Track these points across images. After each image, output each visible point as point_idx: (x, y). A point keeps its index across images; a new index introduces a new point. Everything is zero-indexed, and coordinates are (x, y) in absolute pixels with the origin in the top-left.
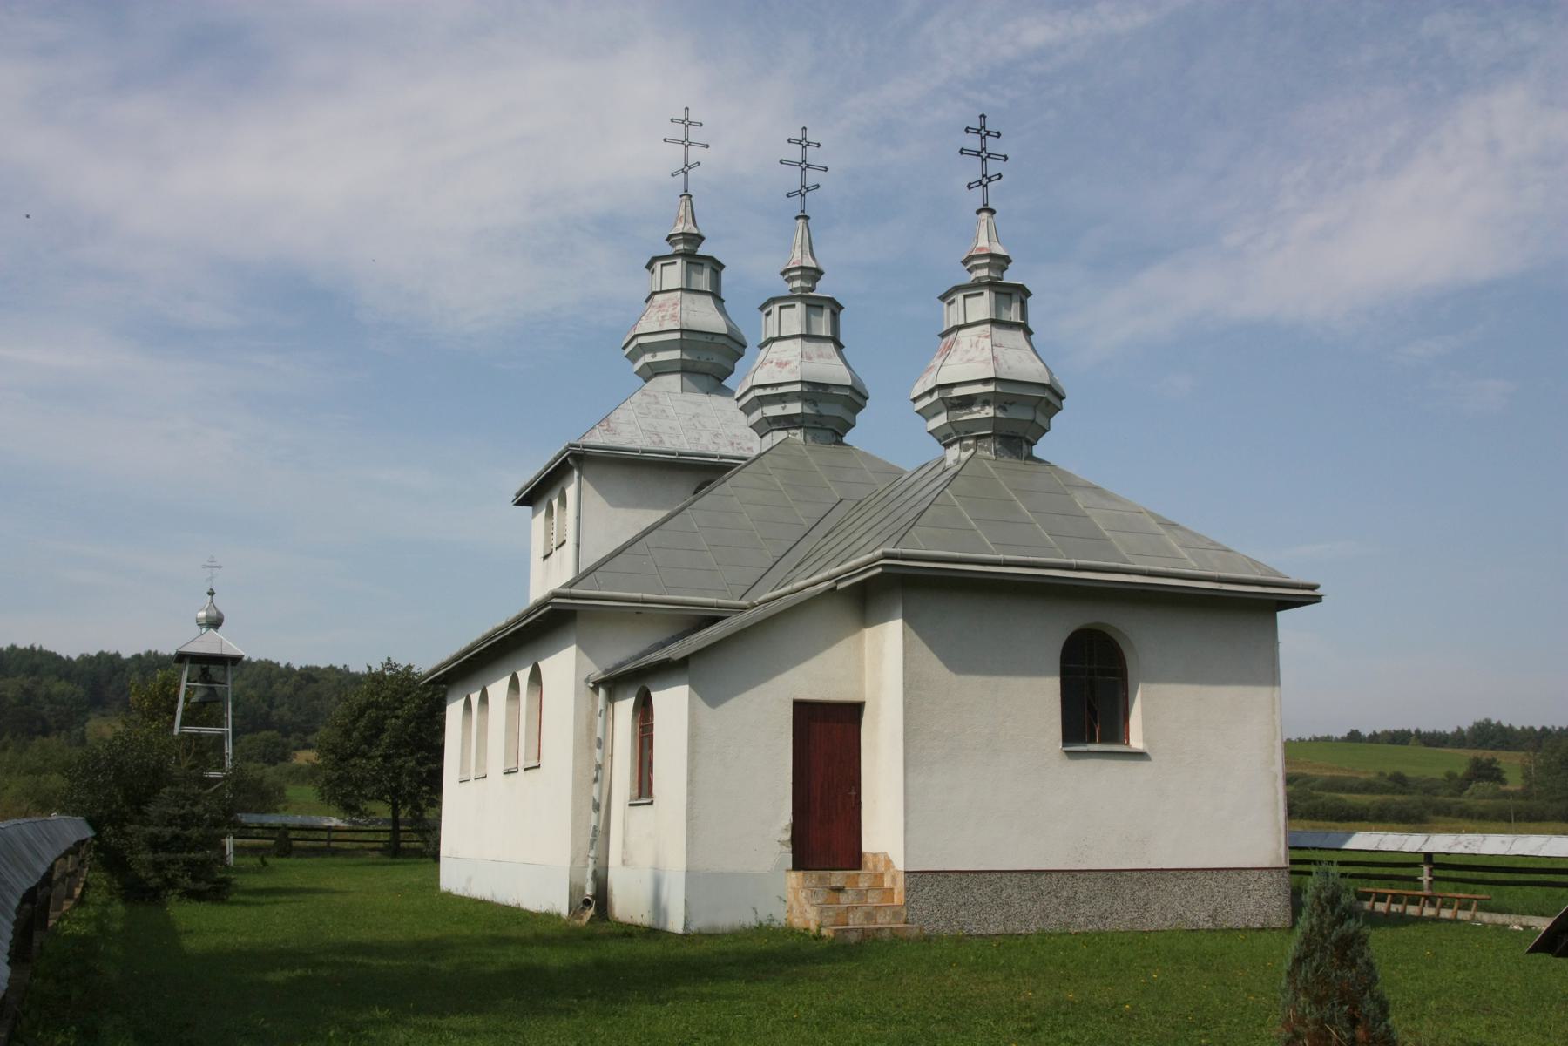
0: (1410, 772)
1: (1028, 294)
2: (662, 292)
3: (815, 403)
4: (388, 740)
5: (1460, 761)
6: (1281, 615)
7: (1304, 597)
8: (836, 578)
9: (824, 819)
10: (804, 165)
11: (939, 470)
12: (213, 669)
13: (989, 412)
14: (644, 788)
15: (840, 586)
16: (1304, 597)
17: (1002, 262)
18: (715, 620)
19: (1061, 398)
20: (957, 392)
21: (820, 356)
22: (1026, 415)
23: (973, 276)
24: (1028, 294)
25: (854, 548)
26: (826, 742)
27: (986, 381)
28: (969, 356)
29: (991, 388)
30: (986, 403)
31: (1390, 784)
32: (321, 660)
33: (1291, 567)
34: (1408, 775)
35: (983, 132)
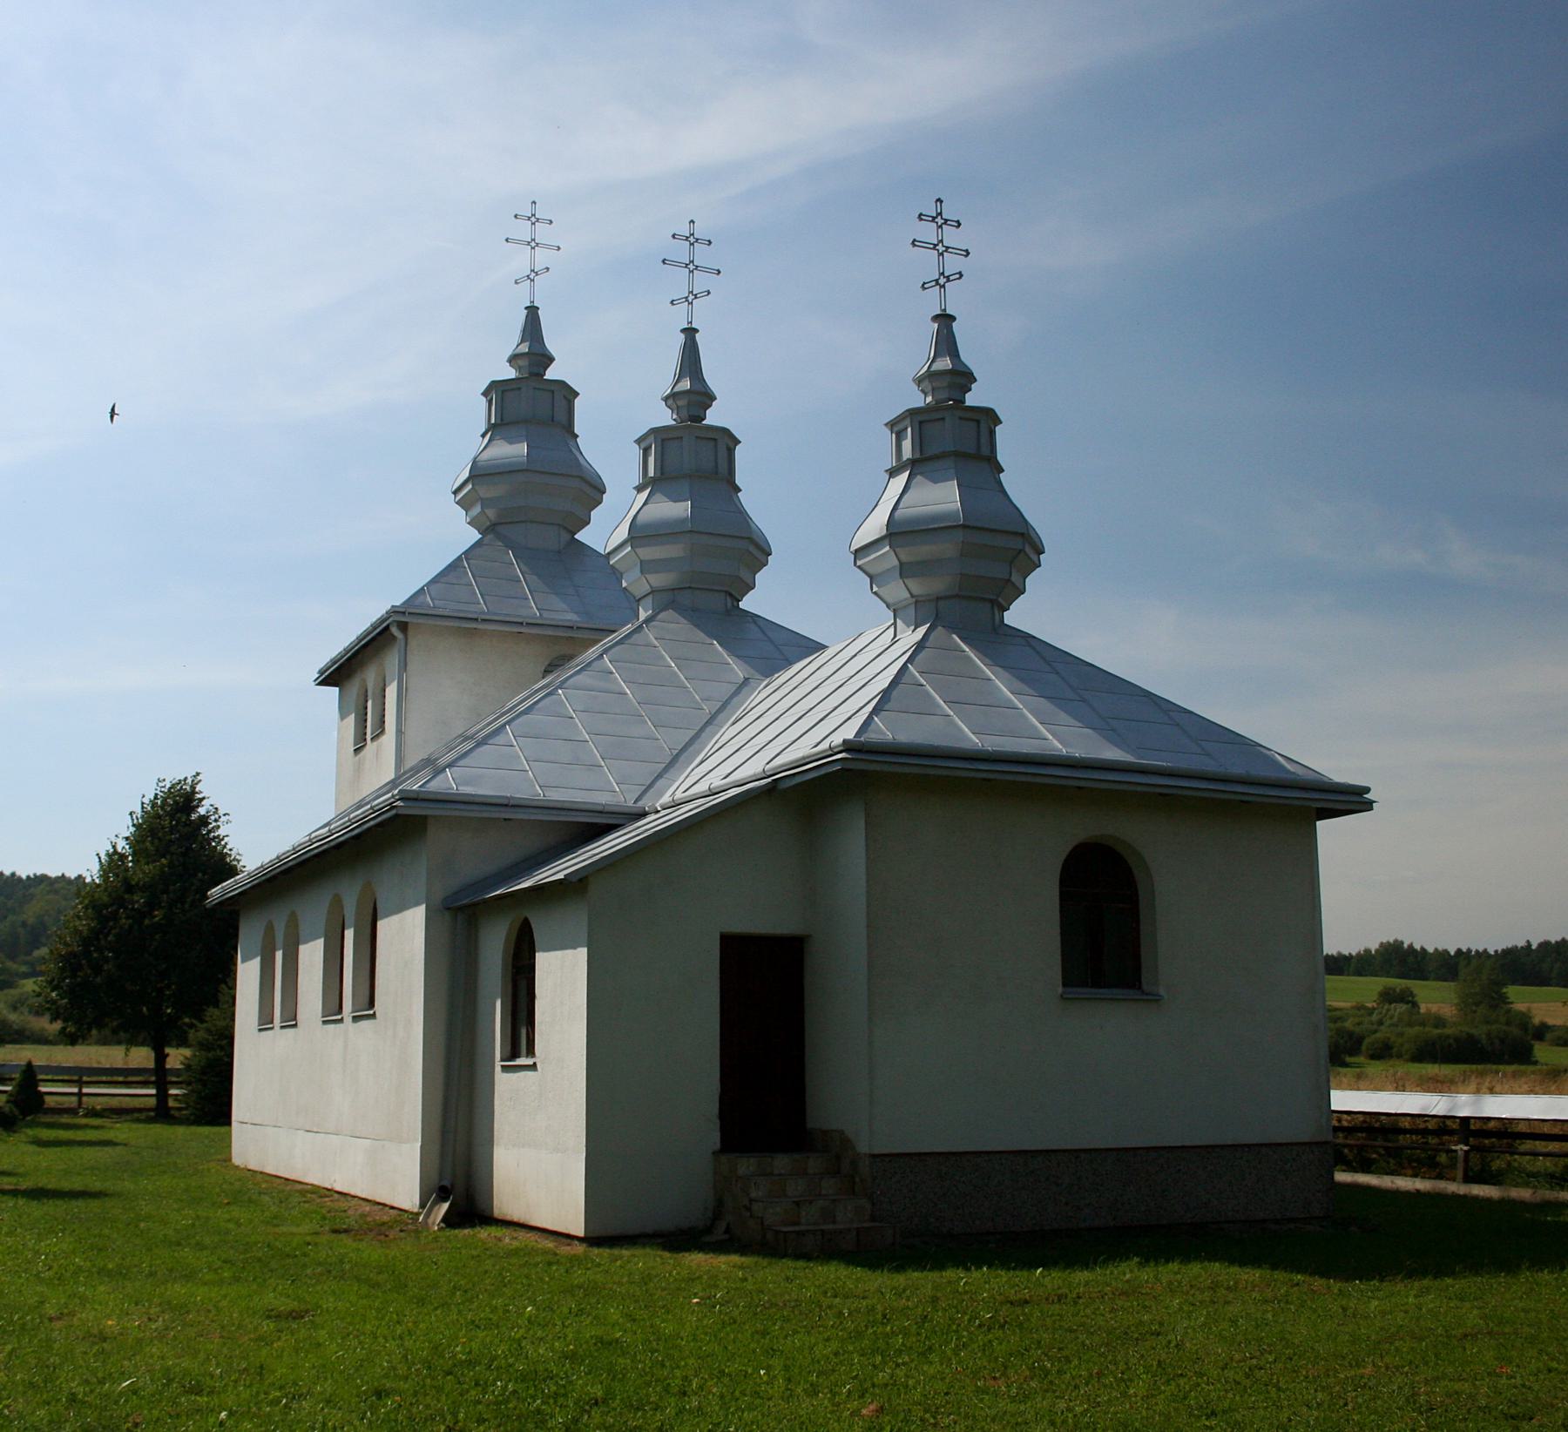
1: (997, 421)
7: (1351, 800)
16: (1351, 800)
24: (997, 421)
33: (1337, 769)
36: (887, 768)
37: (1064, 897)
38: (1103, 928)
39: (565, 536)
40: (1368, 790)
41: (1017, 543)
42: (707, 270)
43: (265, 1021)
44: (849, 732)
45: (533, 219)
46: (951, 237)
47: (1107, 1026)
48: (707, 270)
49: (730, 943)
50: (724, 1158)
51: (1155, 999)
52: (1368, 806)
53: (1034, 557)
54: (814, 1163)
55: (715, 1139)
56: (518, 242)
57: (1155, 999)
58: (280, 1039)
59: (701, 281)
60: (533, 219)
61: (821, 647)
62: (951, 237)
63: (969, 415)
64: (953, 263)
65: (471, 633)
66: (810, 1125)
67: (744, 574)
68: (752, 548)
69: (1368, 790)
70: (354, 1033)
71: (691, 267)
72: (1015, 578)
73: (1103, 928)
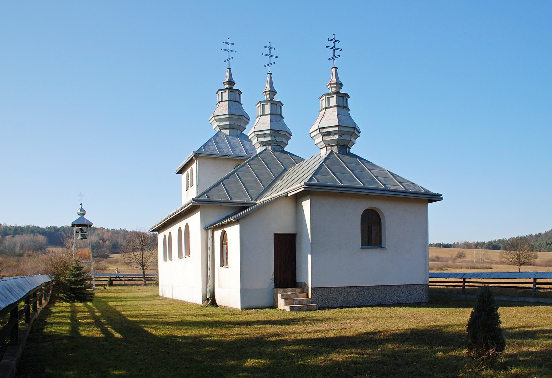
0: (440, 255)
1: (349, 97)
2: (222, 101)
3: (275, 137)
4: (142, 245)
5: (454, 252)
6: (430, 205)
7: (437, 198)
8: (288, 193)
9: (286, 273)
10: (270, 56)
11: (319, 157)
12: (84, 229)
13: (336, 137)
14: (224, 262)
15: (289, 195)
16: (437, 198)
17: (340, 86)
18: (246, 208)
19: (359, 133)
20: (325, 130)
21: (276, 121)
22: (348, 138)
23: (330, 91)
24: (349, 97)
25: (281, 188)
26: (286, 248)
27: (335, 126)
28: (330, 118)
29: (337, 129)
30: (335, 134)
31: (435, 259)
32: (117, 227)
33: (434, 190)
34: (440, 256)
35: (334, 40)
36: (314, 190)
37: (362, 224)
38: (372, 232)
39: (239, 132)
40: (441, 195)
41: (352, 130)
42: (274, 56)
43: (165, 259)
44: (306, 181)
45: (270, 48)
46: (337, 45)
47: (372, 255)
48: (274, 56)
49: (276, 235)
50: (275, 289)
51: (385, 249)
52: (442, 199)
53: (358, 134)
54: (298, 290)
55: (273, 285)
56: (225, 50)
57: (385, 249)
58: (168, 262)
59: (273, 60)
60: (270, 48)
61: (303, 160)
62: (337, 45)
63: (340, 95)
64: (337, 53)
65: (215, 158)
66: (297, 281)
67: (285, 141)
68: (287, 134)
69: (441, 195)
70: (184, 260)
71: (270, 56)
72: (353, 140)
73: (372, 232)
